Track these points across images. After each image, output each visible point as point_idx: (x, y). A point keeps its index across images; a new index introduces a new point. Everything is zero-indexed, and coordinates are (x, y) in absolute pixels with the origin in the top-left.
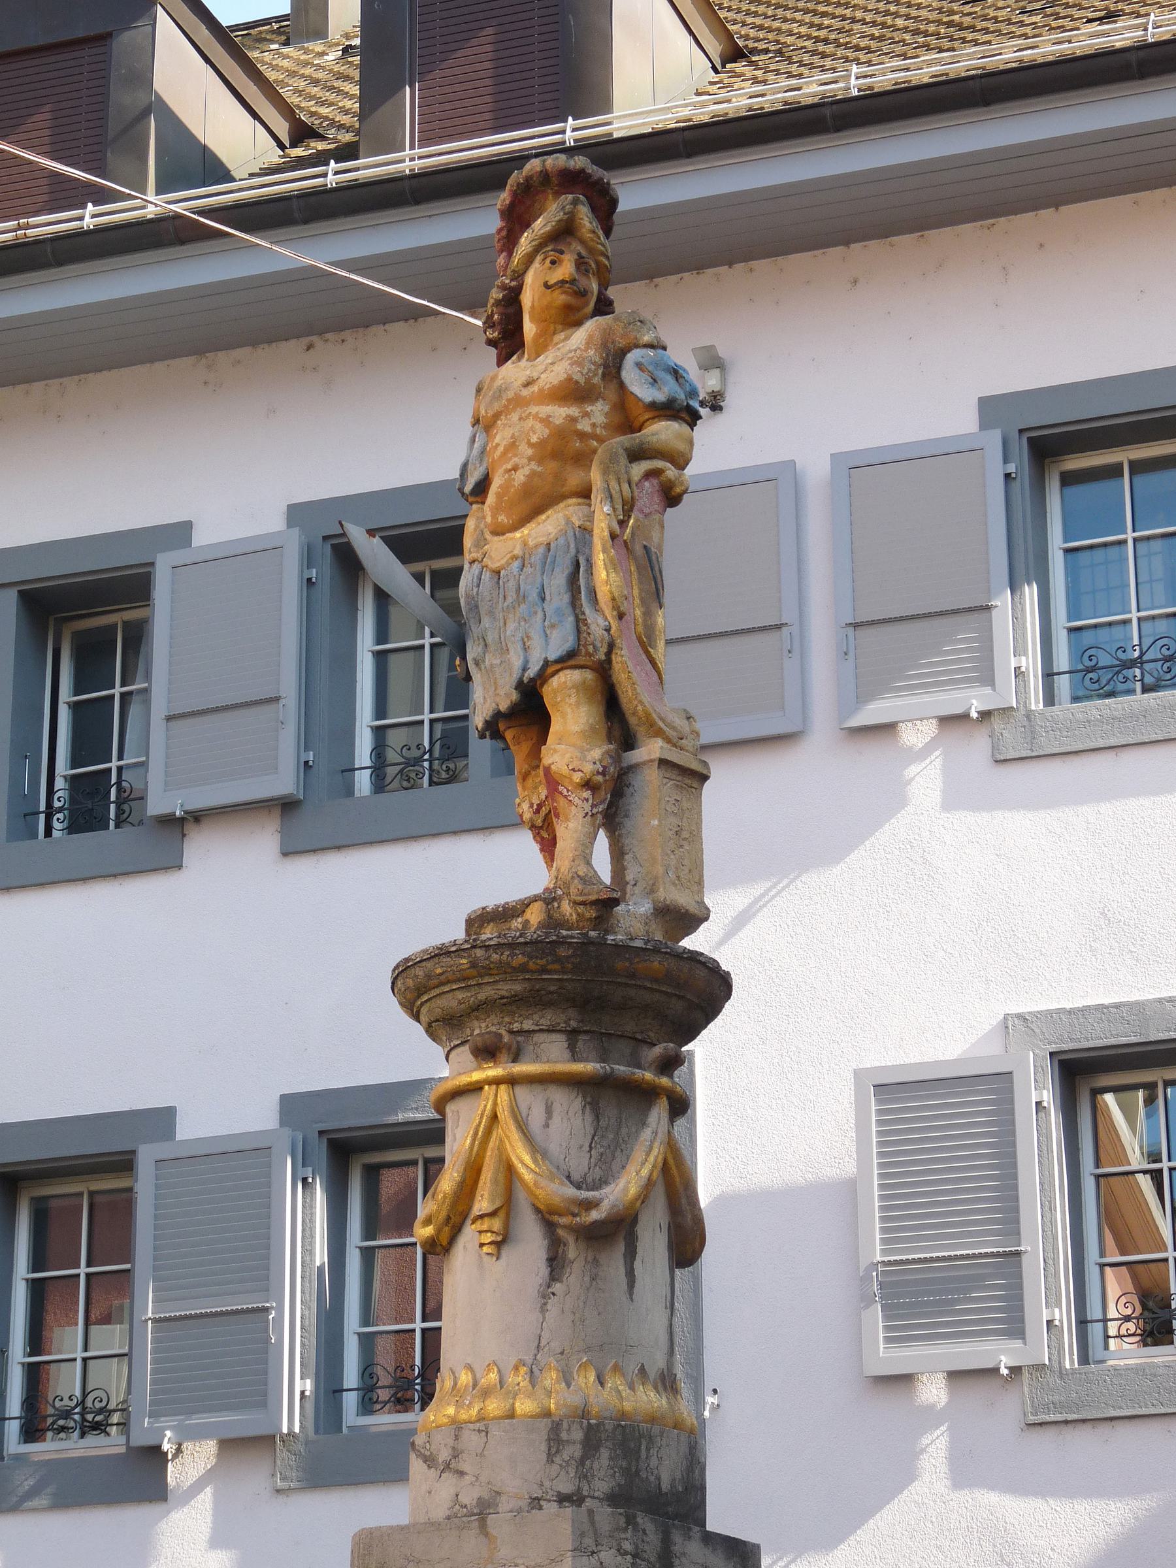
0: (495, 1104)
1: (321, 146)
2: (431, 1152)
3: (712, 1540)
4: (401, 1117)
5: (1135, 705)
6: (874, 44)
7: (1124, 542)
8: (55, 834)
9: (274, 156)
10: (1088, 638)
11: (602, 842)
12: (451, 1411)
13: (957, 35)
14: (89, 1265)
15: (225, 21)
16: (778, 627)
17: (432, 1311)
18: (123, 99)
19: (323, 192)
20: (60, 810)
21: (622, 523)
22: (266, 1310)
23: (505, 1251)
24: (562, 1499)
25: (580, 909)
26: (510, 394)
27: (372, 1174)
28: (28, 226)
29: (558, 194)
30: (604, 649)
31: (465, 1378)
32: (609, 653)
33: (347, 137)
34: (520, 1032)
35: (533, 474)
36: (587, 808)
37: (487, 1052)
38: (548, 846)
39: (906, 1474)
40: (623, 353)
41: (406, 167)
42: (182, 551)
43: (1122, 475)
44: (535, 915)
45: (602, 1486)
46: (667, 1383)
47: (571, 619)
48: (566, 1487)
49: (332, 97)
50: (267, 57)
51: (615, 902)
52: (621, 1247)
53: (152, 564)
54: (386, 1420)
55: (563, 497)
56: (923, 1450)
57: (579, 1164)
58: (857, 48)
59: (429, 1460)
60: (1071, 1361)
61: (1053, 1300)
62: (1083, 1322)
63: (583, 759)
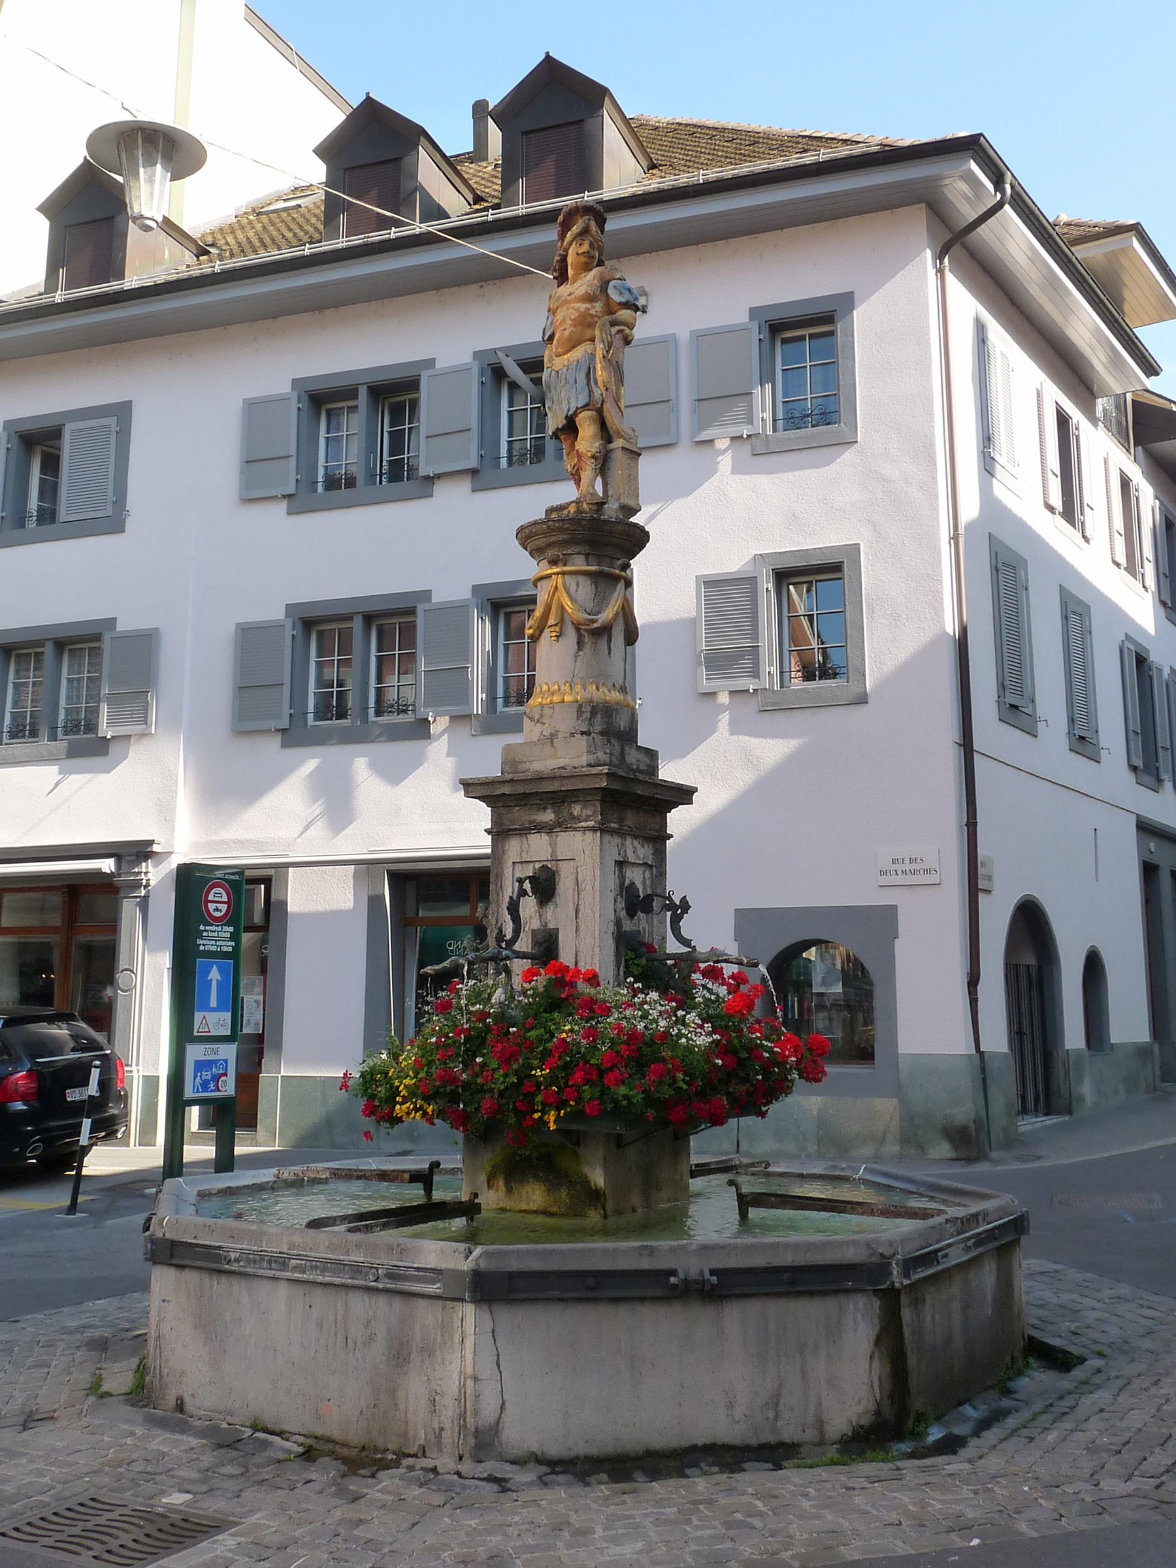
0: (557, 582)
1: (486, 204)
2: (531, 607)
3: (639, 748)
4: (519, 594)
5: (809, 433)
6: (709, 162)
7: (807, 399)
8: (383, 483)
9: (467, 209)
10: (791, 406)
11: (599, 480)
12: (540, 700)
13: (743, 158)
14: (399, 650)
15: (448, 155)
16: (668, 401)
17: (532, 667)
18: (406, 185)
19: (487, 222)
20: (385, 474)
21: (608, 352)
22: (468, 667)
23: (560, 638)
24: (583, 733)
25: (590, 506)
26: (563, 299)
27: (508, 616)
28: (368, 237)
29: (582, 216)
30: (600, 403)
31: (545, 688)
32: (602, 405)
33: (496, 201)
34: (566, 554)
35: (572, 331)
36: (593, 465)
37: (554, 562)
38: (578, 482)
39: (713, 729)
40: (609, 282)
41: (520, 212)
42: (431, 370)
43: (805, 340)
44: (572, 509)
45: (598, 728)
46: (623, 690)
47: (587, 390)
48: (584, 729)
49: (489, 184)
50: (464, 168)
51: (605, 503)
52: (605, 639)
53: (420, 376)
54: (514, 709)
55: (585, 341)
56: (719, 721)
57: (590, 606)
58: (702, 164)
59: (531, 719)
60: (777, 687)
61: (771, 664)
62: (782, 673)
63: (592, 447)
